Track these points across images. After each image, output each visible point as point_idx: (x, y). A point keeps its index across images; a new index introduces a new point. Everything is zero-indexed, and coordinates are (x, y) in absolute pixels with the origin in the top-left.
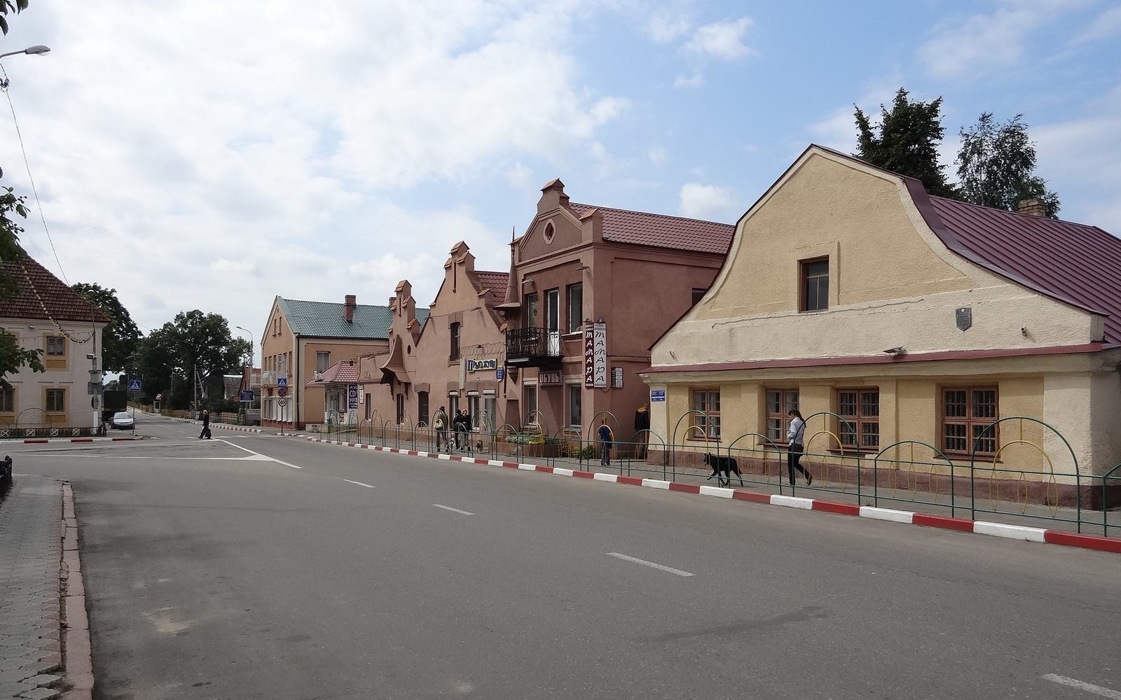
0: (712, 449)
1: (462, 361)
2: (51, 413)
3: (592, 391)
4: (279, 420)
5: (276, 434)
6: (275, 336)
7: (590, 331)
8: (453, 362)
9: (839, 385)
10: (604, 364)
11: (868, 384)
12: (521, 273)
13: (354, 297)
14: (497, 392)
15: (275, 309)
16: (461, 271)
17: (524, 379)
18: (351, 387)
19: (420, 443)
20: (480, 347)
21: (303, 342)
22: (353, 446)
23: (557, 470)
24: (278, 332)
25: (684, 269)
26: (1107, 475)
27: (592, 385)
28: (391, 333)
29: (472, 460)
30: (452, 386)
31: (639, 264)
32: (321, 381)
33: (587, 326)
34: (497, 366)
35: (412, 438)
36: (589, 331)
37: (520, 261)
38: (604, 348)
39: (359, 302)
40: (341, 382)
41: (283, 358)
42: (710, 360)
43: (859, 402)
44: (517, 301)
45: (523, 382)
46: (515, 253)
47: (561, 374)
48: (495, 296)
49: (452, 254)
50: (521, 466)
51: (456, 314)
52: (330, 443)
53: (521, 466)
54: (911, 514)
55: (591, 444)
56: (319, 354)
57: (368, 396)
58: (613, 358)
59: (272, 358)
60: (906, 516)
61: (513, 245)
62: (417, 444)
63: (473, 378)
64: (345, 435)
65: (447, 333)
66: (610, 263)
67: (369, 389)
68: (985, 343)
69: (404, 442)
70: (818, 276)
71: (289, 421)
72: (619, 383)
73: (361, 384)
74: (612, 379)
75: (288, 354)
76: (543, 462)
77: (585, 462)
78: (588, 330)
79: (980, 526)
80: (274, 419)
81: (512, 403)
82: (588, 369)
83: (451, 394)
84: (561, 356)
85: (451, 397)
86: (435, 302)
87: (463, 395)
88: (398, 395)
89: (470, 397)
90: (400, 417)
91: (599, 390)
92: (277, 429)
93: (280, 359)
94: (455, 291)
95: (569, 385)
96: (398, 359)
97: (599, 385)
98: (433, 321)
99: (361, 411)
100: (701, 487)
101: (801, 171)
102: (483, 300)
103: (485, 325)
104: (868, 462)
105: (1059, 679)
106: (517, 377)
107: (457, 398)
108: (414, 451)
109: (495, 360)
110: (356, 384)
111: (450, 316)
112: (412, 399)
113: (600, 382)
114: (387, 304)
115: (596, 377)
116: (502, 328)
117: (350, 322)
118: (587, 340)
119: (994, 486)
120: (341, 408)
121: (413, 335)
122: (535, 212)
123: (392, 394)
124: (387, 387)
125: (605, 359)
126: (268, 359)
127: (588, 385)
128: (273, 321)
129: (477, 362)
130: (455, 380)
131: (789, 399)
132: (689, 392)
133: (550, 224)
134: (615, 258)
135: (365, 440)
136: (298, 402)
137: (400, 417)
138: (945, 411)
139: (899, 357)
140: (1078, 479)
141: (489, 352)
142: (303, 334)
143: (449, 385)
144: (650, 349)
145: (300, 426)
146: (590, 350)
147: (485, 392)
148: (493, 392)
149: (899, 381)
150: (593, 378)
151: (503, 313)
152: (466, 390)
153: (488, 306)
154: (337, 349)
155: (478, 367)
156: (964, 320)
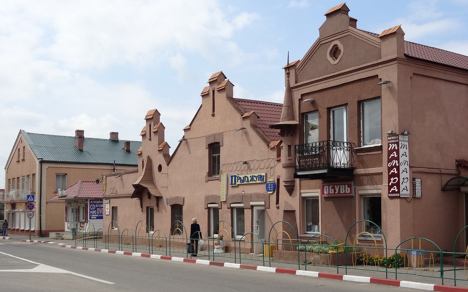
1: (223, 177)
3: (398, 201)
4: (27, 229)
5: (26, 241)
6: (18, 162)
7: (395, 143)
8: (210, 178)
10: (407, 175)
12: (297, 95)
13: (82, 132)
14: (267, 204)
15: (19, 140)
16: (220, 98)
17: (302, 191)
19: (100, 243)
21: (45, 166)
24: (21, 158)
26: (397, 248)
27: (398, 195)
29: (122, 252)
30: (210, 200)
31: (431, 81)
32: (65, 197)
35: (162, 245)
36: (392, 143)
37: (296, 82)
38: (407, 159)
39: (86, 136)
40: (82, 198)
41: (26, 179)
44: (293, 119)
45: (300, 193)
48: (258, 117)
49: (210, 83)
50: (346, 277)
51: (214, 135)
52: (87, 249)
55: (399, 252)
56: (58, 175)
57: (114, 209)
58: (414, 169)
59: (16, 180)
60: (367, 279)
61: (288, 68)
63: (233, 192)
64: (92, 242)
65: (205, 153)
67: (115, 202)
69: (158, 249)
71: (32, 229)
72: (418, 194)
73: (106, 199)
75: (31, 177)
76: (332, 270)
78: (389, 142)
80: (17, 228)
81: (289, 213)
82: (392, 179)
83: (209, 206)
85: (209, 209)
86: (190, 125)
87: (225, 206)
88: (147, 208)
89: (232, 209)
90: (150, 224)
92: (26, 236)
93: (23, 180)
94: (213, 115)
95: (361, 196)
96: (149, 176)
98: (187, 143)
99: (107, 220)
103: (250, 144)
108: (168, 256)
109: (264, 174)
110: (101, 199)
111: (208, 137)
112: (164, 211)
113: (405, 192)
115: (402, 187)
117: (81, 150)
120: (81, 219)
122: (316, 36)
123: (142, 207)
125: (408, 171)
126: (11, 180)
127: (391, 195)
128: (17, 150)
129: (242, 176)
130: (215, 193)
134: (414, 74)
135: (129, 249)
136: (40, 214)
137: (150, 224)
141: (256, 168)
142: (45, 159)
143: (207, 198)
145: (43, 234)
146: (395, 162)
148: (263, 203)
150: (398, 188)
152: (229, 201)
153: (254, 127)
154: (72, 171)
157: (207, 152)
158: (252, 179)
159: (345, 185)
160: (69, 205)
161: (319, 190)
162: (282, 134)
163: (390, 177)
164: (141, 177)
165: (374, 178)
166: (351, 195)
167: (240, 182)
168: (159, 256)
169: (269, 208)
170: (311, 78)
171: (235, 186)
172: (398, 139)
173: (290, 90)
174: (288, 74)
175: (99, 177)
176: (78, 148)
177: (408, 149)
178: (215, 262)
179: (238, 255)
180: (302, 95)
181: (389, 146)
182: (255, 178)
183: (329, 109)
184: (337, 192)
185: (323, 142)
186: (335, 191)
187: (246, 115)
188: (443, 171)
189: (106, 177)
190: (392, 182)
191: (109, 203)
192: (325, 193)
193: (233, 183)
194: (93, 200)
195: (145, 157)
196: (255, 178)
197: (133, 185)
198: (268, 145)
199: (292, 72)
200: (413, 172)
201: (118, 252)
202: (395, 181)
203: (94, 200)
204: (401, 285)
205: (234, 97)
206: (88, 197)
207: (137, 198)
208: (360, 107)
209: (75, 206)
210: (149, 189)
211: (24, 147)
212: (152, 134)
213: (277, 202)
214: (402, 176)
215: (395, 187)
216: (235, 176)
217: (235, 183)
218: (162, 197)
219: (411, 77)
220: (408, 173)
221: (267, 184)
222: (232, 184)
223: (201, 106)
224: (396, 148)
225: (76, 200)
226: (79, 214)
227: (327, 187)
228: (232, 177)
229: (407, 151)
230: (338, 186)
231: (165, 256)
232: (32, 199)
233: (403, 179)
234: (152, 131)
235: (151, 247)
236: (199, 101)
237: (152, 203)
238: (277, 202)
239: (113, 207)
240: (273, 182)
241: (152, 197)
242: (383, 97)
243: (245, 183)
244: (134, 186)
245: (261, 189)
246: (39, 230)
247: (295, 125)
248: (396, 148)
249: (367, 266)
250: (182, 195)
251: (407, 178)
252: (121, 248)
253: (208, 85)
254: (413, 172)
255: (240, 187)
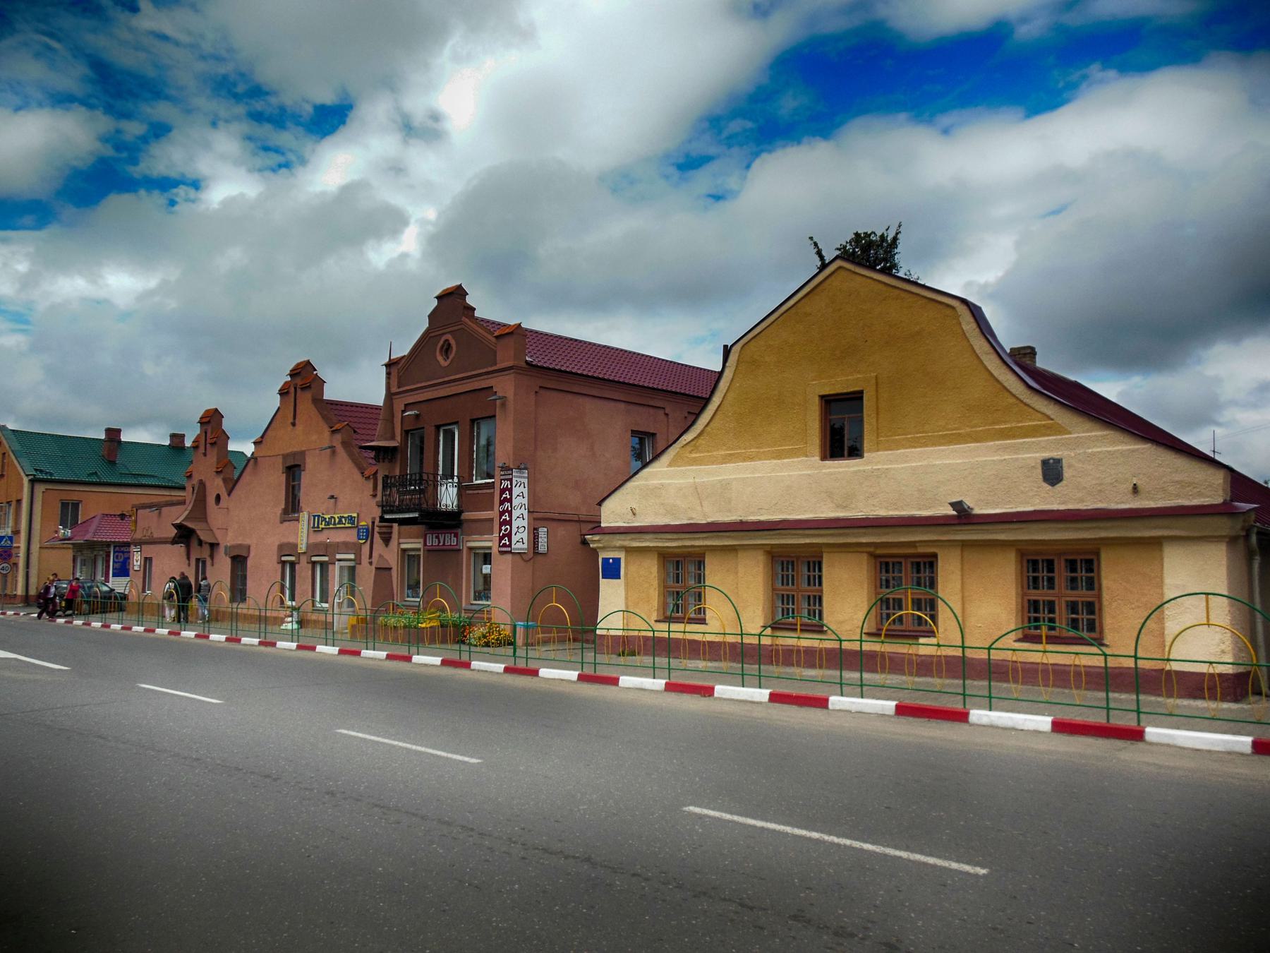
0: (1087, 657)
1: (304, 516)
2: (819, 594)
3: (509, 557)
7: (507, 480)
9: (879, 552)
10: (525, 523)
11: (921, 550)
18: (117, 548)
20: (332, 497)
21: (40, 489)
22: (130, 629)
23: (75, 622)
25: (622, 406)
28: (190, 477)
31: (570, 397)
33: (502, 473)
34: (358, 523)
35: (263, 621)
36: (504, 480)
38: (525, 501)
42: (692, 519)
43: (907, 573)
44: (393, 438)
46: (392, 377)
47: (459, 534)
48: (355, 432)
49: (291, 375)
50: (416, 659)
53: (416, 659)
54: (225, 636)
57: (148, 561)
58: (536, 515)
61: (388, 365)
62: (144, 620)
66: (534, 393)
67: (150, 550)
68: (1082, 501)
70: (847, 416)
72: (542, 548)
74: (534, 542)
75: (14, 504)
76: (453, 652)
77: (104, 615)
78: (502, 477)
79: (1152, 732)
81: (383, 571)
82: (503, 528)
84: (460, 513)
86: (262, 437)
87: (304, 559)
88: (198, 560)
89: (314, 563)
91: (518, 556)
94: (294, 424)
95: (471, 549)
97: (518, 549)
100: (621, 678)
101: (821, 288)
102: (338, 437)
104: (925, 647)
105: (697, 810)
106: (391, 537)
107: (293, 564)
108: (206, 633)
110: (128, 545)
111: (285, 457)
113: (520, 545)
114: (167, 443)
115: (514, 539)
116: (367, 473)
118: (503, 491)
119: (939, 664)
121: (225, 480)
123: (188, 558)
124: (180, 549)
125: (526, 516)
131: (692, 568)
132: (658, 557)
133: (447, 340)
134: (541, 387)
138: (878, 585)
139: (963, 516)
140: (963, 651)
144: (600, 504)
147: (338, 556)
148: (352, 556)
149: (965, 545)
150: (510, 540)
151: (372, 454)
153: (345, 444)
155: (328, 523)
156: (1052, 472)
157: (283, 477)
158: (340, 522)
159: (451, 534)
160: (79, 553)
161: (422, 540)
162: (377, 458)
163: (501, 524)
164: (187, 512)
165: (484, 527)
166: (457, 547)
167: (325, 525)
168: (223, 638)
169: (360, 564)
170: (418, 382)
171: (317, 530)
172: (512, 474)
173: (390, 396)
174: (388, 374)
175: (127, 509)
176: (106, 457)
177: (527, 488)
178: (267, 641)
179: (263, 626)
180: (406, 405)
181: (501, 483)
182: (343, 520)
183: (473, 421)
184: (441, 544)
185: (415, 474)
186: (439, 542)
187: (337, 426)
188: (582, 518)
189: (137, 510)
190: (503, 531)
191: (140, 551)
192: (428, 544)
193: (316, 525)
194: (119, 546)
195: (195, 481)
196: (343, 520)
197: (173, 524)
198: (362, 473)
199: (394, 370)
200: (535, 519)
201: (135, 628)
202: (506, 530)
203: (122, 546)
204: (1148, 737)
205: (326, 397)
206: (111, 541)
207: (182, 545)
208: (473, 427)
209: (87, 553)
210: (198, 532)
211: (4, 454)
212: (208, 445)
213: (371, 556)
214: (515, 524)
215: (506, 538)
216: (319, 516)
217: (318, 527)
218: (218, 544)
219: (536, 392)
220: (526, 520)
221: (359, 530)
222: (314, 527)
223: (279, 408)
224: (509, 486)
225: (91, 545)
226: (95, 568)
227: (431, 535)
228: (314, 516)
229: (526, 491)
230: (443, 535)
231: (202, 633)
232: (9, 542)
233: (518, 527)
234: (208, 441)
235: (234, 624)
236: (276, 401)
237: (205, 553)
238: (371, 556)
239: (146, 558)
240: (366, 527)
241: (203, 544)
242: (497, 417)
243: (331, 526)
244: (176, 526)
245: (351, 536)
246: (24, 594)
247: (395, 448)
248: (509, 486)
249: (506, 646)
250: (247, 542)
251: (524, 527)
252: (120, 621)
253: (289, 379)
254: (535, 519)
255: (325, 531)
